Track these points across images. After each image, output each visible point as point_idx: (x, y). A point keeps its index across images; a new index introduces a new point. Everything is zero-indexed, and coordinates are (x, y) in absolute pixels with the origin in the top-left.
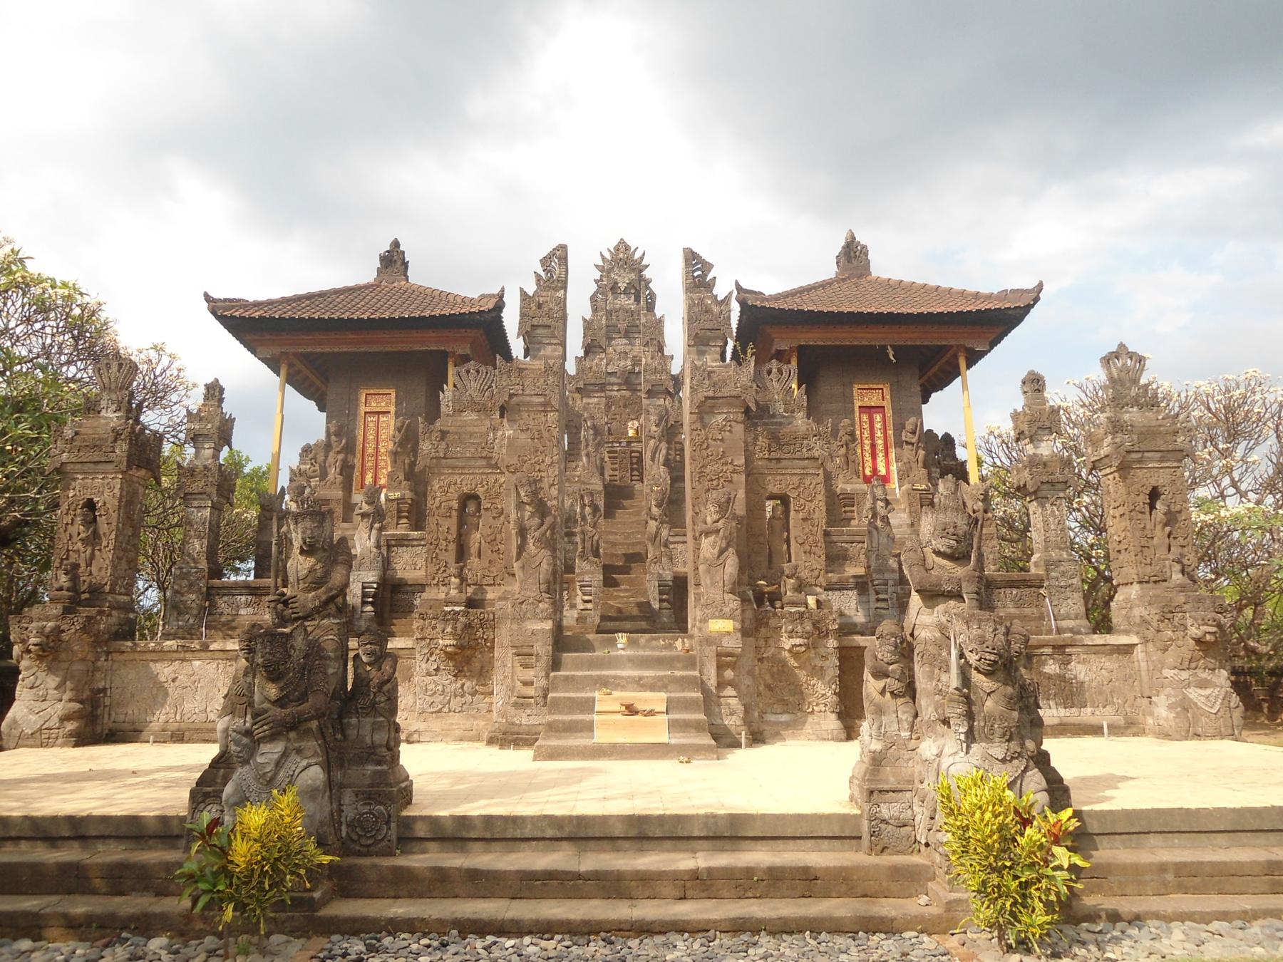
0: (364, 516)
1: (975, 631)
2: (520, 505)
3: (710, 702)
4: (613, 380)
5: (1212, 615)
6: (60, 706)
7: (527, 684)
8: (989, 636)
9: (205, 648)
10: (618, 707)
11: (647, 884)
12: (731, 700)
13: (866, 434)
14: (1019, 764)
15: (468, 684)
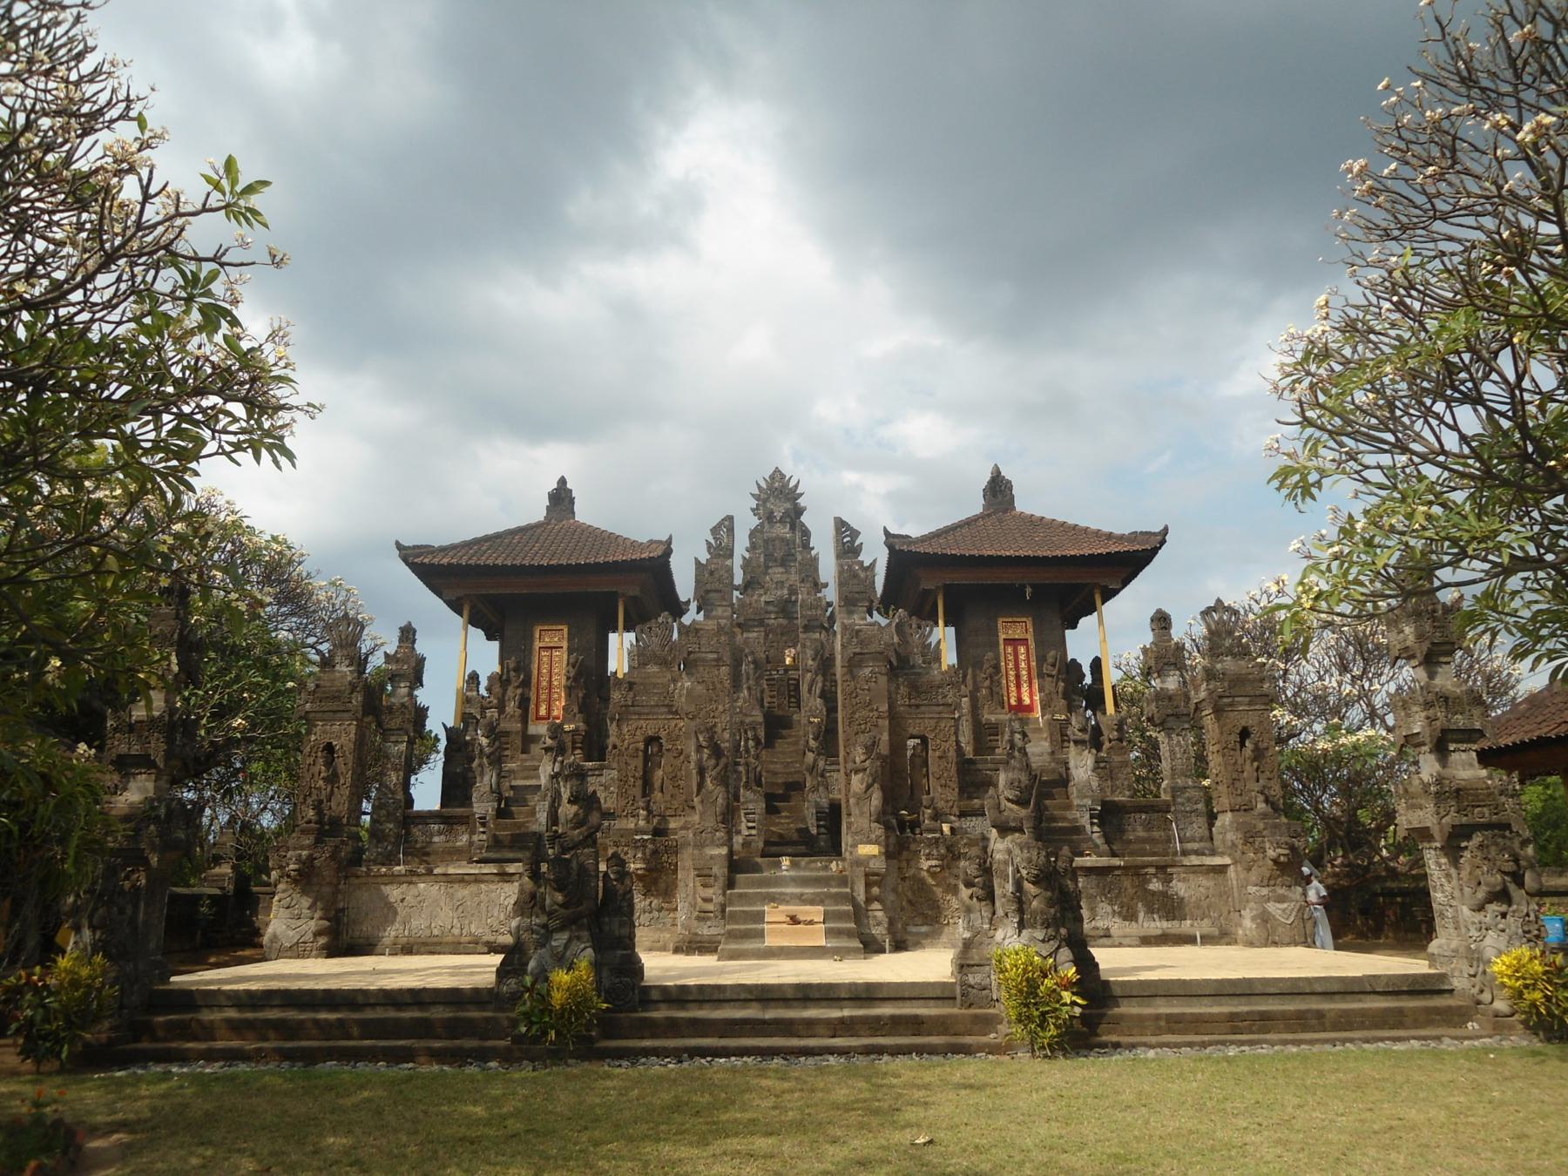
0: (547, 750)
1: (1026, 855)
2: (699, 748)
3: (859, 915)
4: (771, 608)
5: (1287, 839)
6: (312, 923)
7: (706, 900)
8: (1035, 858)
10: (784, 919)
11: (810, 1026)
12: (878, 912)
13: (1011, 665)
14: (1054, 944)
15: (655, 902)
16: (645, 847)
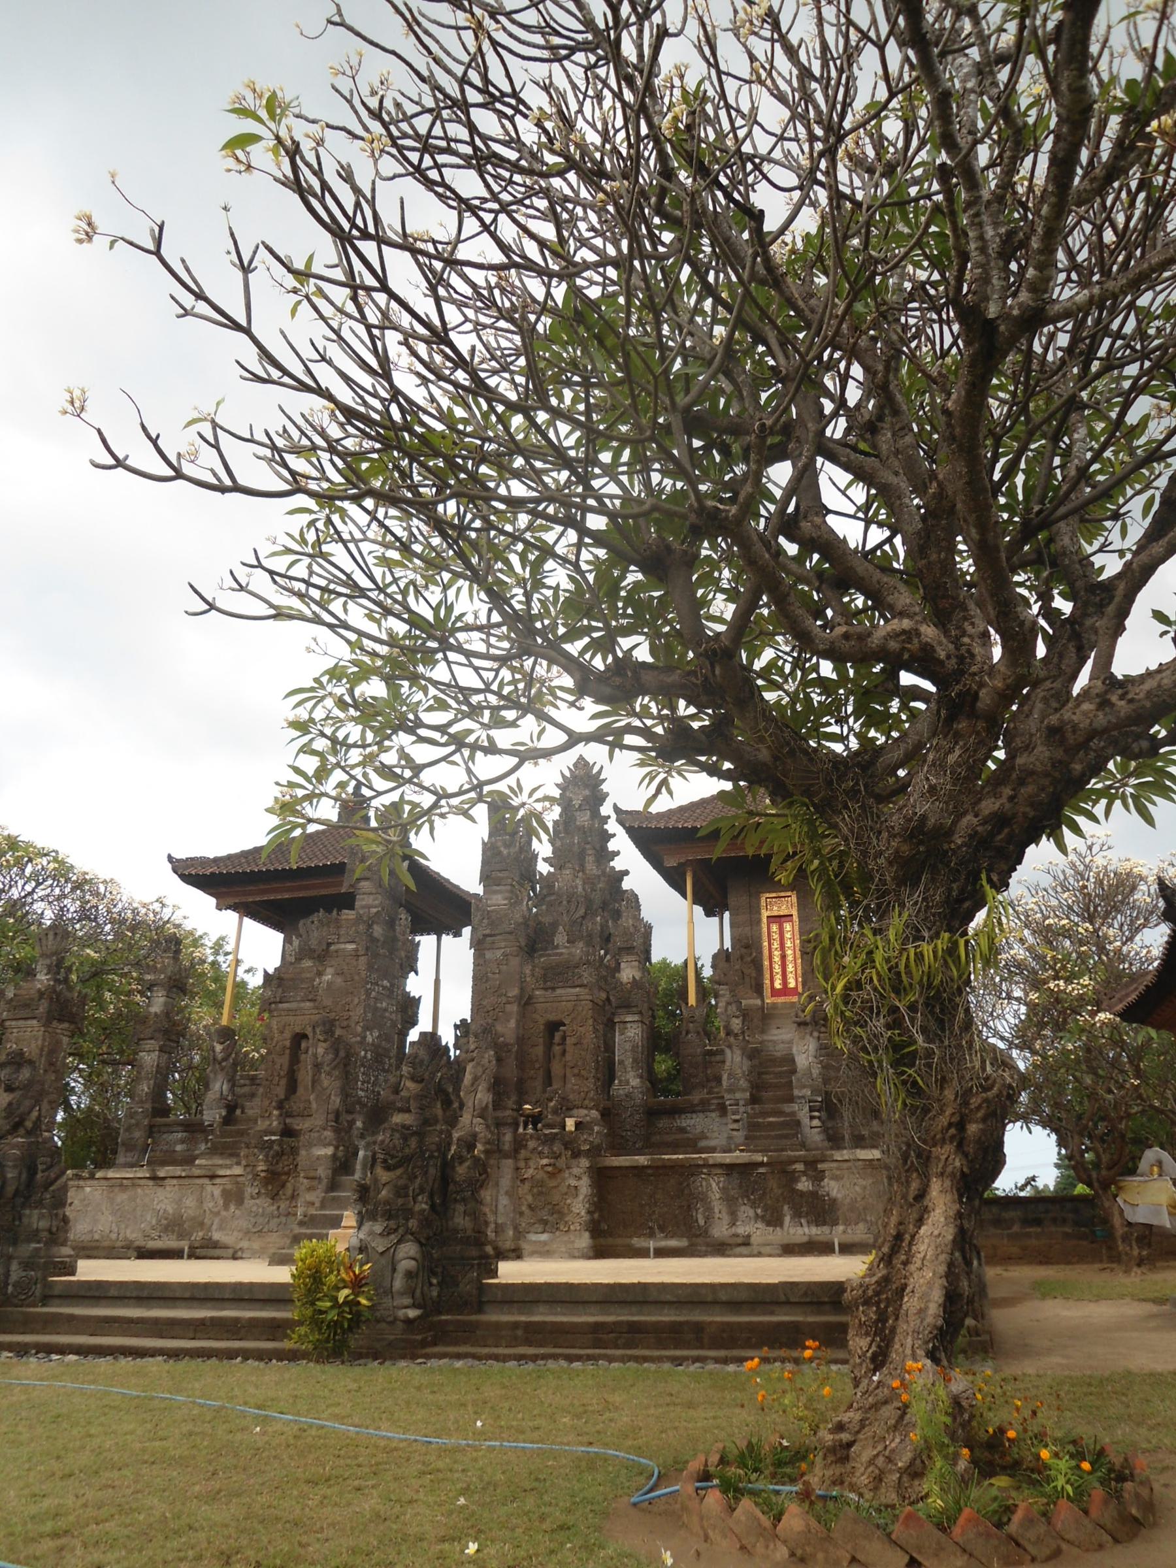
9: (92, 1177)
13: (776, 945)
16: (271, 1148)
